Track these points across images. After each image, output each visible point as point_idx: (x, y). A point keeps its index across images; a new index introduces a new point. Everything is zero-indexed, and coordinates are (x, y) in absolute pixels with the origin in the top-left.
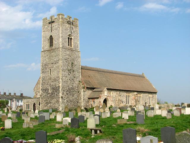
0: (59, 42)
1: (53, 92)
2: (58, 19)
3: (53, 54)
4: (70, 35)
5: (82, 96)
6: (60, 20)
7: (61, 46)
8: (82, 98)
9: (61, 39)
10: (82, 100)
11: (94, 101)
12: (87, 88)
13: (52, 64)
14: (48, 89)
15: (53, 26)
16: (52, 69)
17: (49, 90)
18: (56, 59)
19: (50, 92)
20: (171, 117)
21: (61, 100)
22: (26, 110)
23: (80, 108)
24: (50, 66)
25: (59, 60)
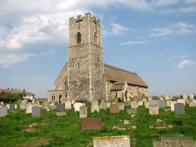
0: (87, 38)
1: (82, 84)
2: (86, 18)
3: (81, 49)
4: (96, 32)
5: (107, 88)
6: (88, 19)
7: (89, 42)
8: (107, 90)
9: (89, 36)
10: (107, 92)
11: (116, 93)
12: (110, 81)
13: (81, 58)
14: (77, 82)
15: (81, 24)
16: (80, 63)
17: (78, 83)
18: (84, 54)
19: (78, 84)
20: (85, 104)
21: (91, 91)
22: (51, 101)
23: (105, 99)
24: (78, 60)
25: (88, 55)
